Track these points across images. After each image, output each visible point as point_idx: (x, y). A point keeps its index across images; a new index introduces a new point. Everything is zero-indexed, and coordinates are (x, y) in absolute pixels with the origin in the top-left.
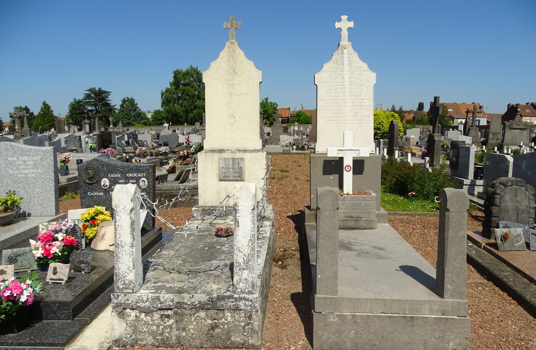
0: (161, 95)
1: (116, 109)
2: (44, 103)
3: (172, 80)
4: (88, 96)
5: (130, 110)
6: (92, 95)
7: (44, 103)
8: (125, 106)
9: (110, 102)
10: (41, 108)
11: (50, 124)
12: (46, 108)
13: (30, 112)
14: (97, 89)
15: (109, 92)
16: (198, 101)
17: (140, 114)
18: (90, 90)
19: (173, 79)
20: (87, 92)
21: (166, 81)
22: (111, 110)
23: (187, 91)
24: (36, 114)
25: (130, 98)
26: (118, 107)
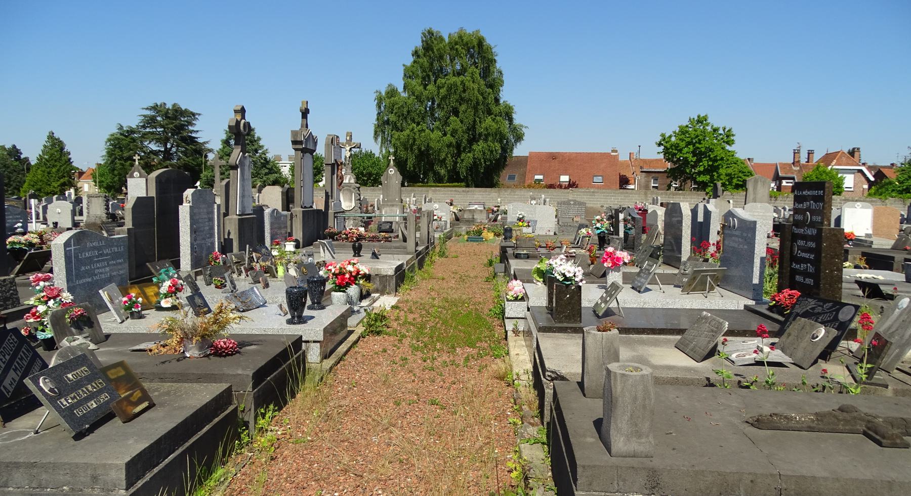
1: (211, 151)
2: (51, 136)
4: (150, 121)
6: (159, 119)
7: (51, 136)
9: (193, 135)
10: (45, 146)
11: (62, 180)
13: (22, 157)
14: (169, 106)
15: (194, 114)
16: (489, 120)
18: (155, 108)
20: (148, 113)
21: (391, 70)
22: (197, 150)
24: (33, 161)
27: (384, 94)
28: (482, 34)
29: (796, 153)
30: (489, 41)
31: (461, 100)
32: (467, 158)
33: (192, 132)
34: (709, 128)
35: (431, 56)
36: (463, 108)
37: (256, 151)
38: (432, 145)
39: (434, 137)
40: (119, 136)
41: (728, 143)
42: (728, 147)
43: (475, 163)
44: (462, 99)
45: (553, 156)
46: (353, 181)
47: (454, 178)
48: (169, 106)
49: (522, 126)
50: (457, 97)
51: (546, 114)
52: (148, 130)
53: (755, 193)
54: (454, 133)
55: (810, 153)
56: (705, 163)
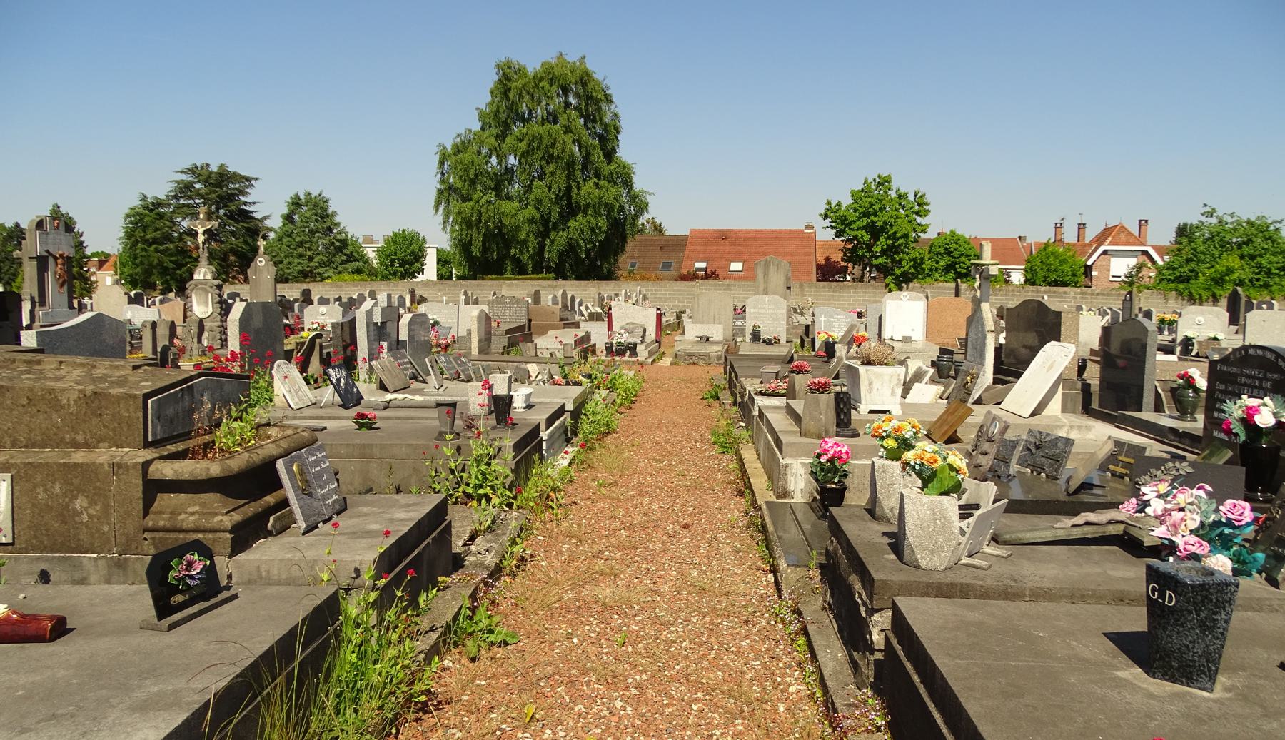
0: (437, 158)
1: (271, 230)
3: (483, 99)
4: (185, 189)
5: (312, 232)
6: (198, 186)
8: (296, 217)
12: (17, 225)
14: (214, 168)
15: (248, 179)
17: (344, 243)
18: (193, 171)
19: (489, 98)
20: (184, 177)
21: (462, 111)
22: (252, 228)
23: (545, 141)
25: (314, 194)
26: (276, 222)
27: (449, 148)
28: (590, 66)
29: (1059, 227)
30: (600, 71)
31: (550, 158)
32: (559, 240)
33: (245, 203)
34: (893, 194)
35: (512, 98)
36: (552, 167)
37: (330, 230)
38: (506, 221)
39: (514, 212)
40: (142, 210)
41: (917, 213)
42: (919, 219)
43: (571, 245)
44: (551, 156)
45: (723, 235)
46: (209, 277)
47: (538, 267)
48: (214, 168)
49: (643, 192)
50: (540, 153)
51: (678, 176)
52: (182, 201)
53: (765, 282)
54: (539, 202)
55: (1081, 227)
56: (883, 241)
